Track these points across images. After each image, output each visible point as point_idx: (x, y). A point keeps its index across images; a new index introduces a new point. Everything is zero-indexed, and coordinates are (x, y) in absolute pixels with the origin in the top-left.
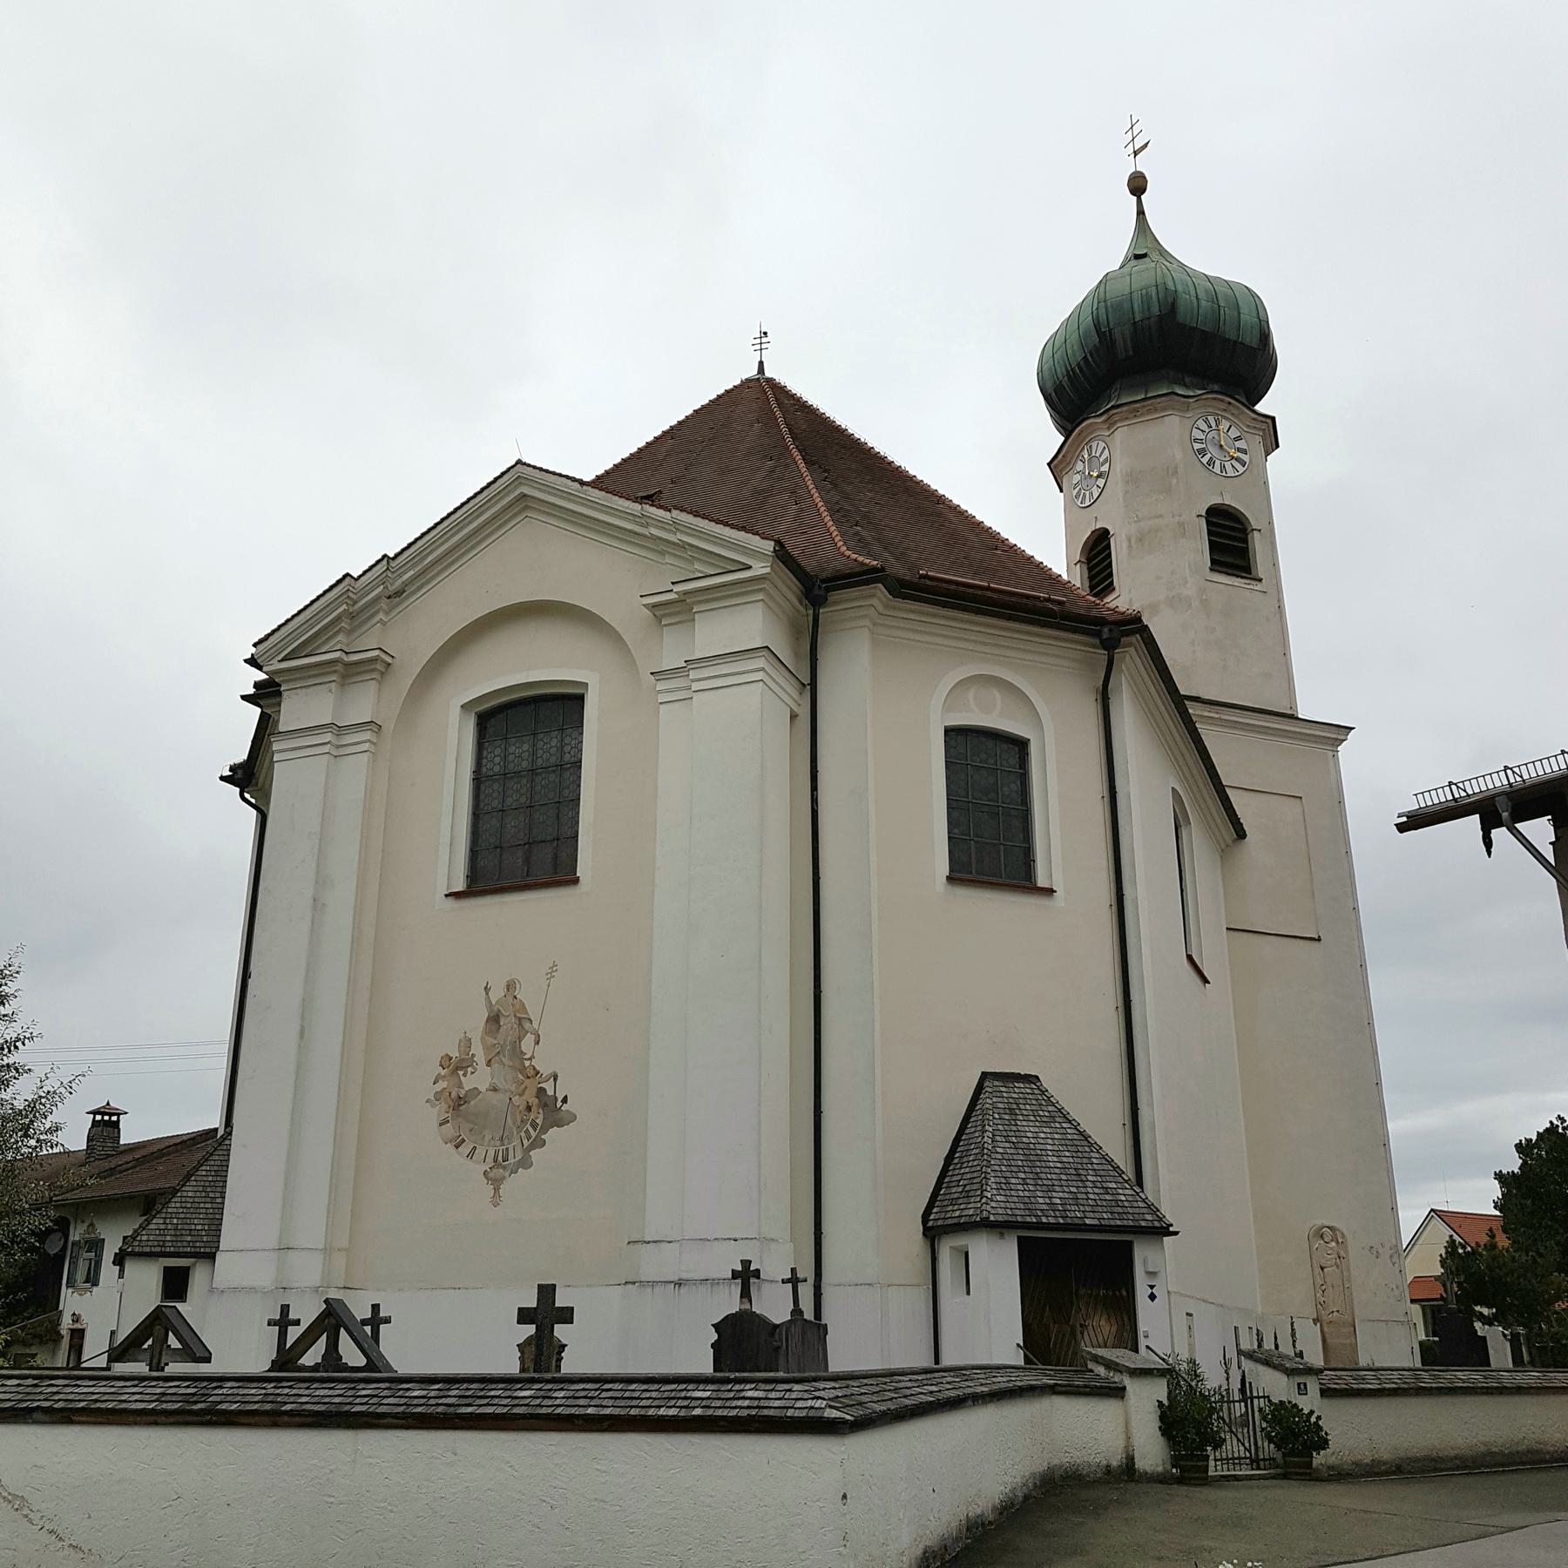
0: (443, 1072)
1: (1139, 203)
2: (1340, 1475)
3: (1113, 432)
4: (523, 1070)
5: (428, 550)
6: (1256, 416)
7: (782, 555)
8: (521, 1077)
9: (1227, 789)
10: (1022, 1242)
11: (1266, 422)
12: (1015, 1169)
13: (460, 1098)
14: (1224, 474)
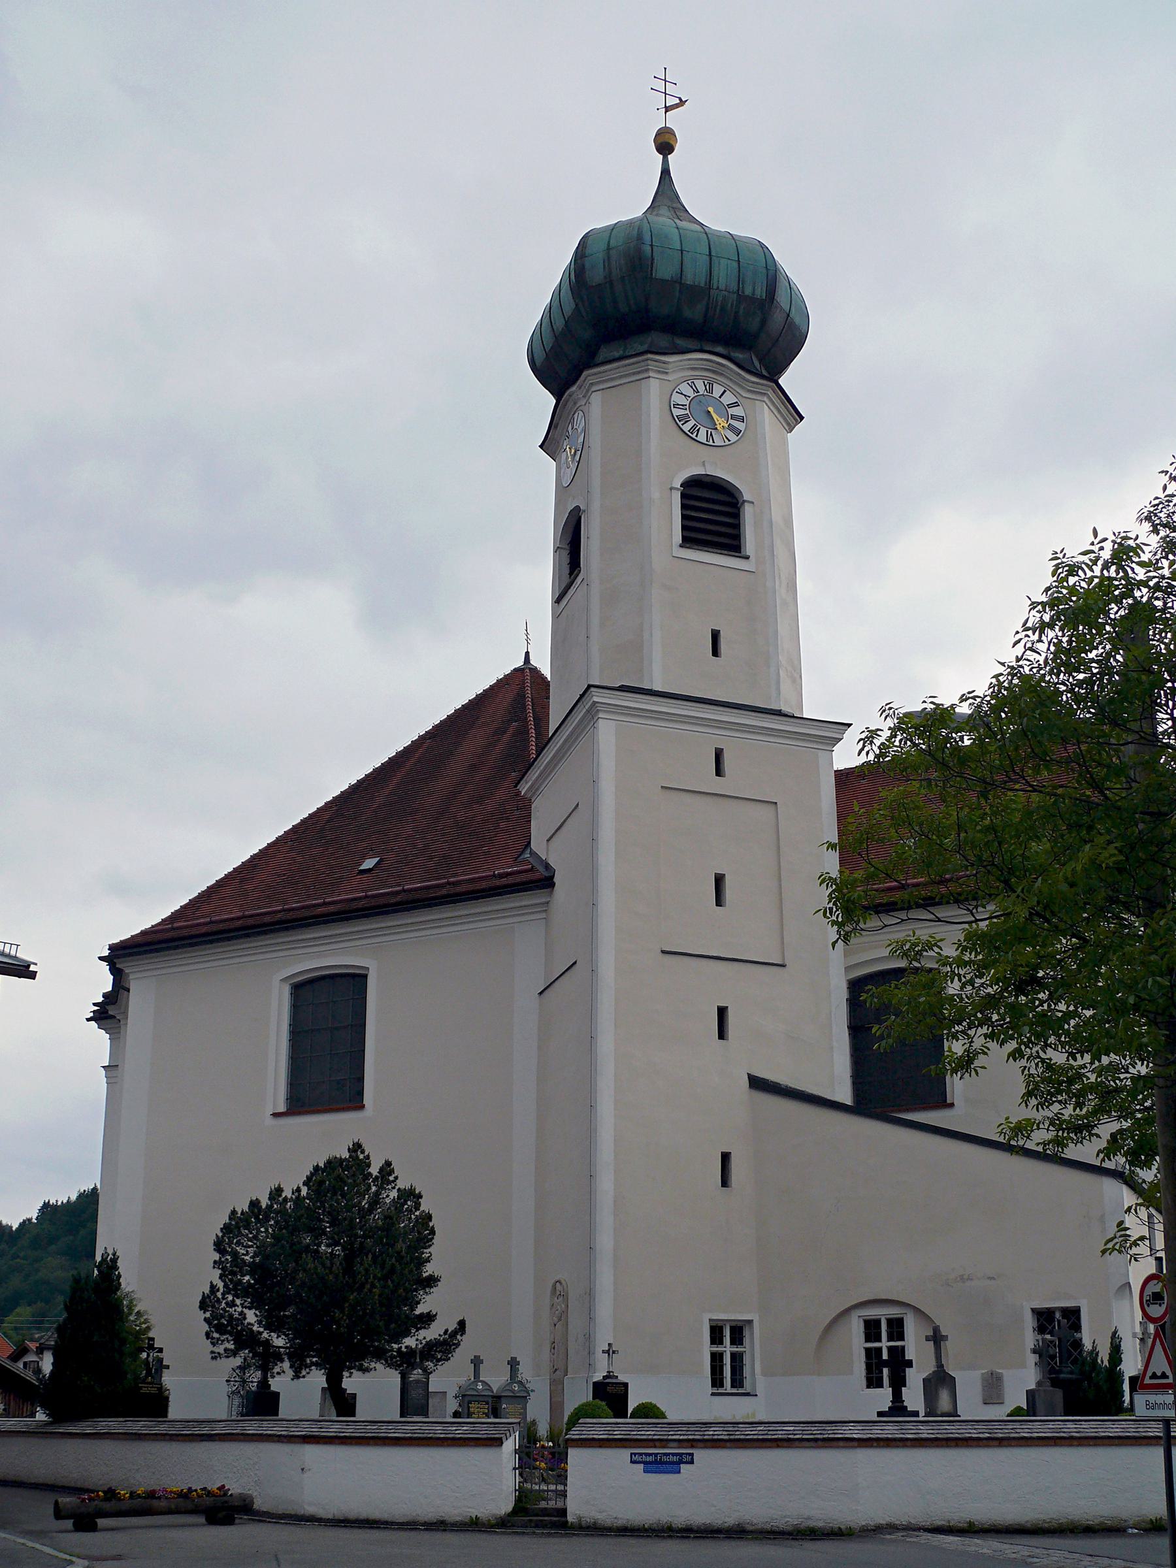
1: (665, 162)
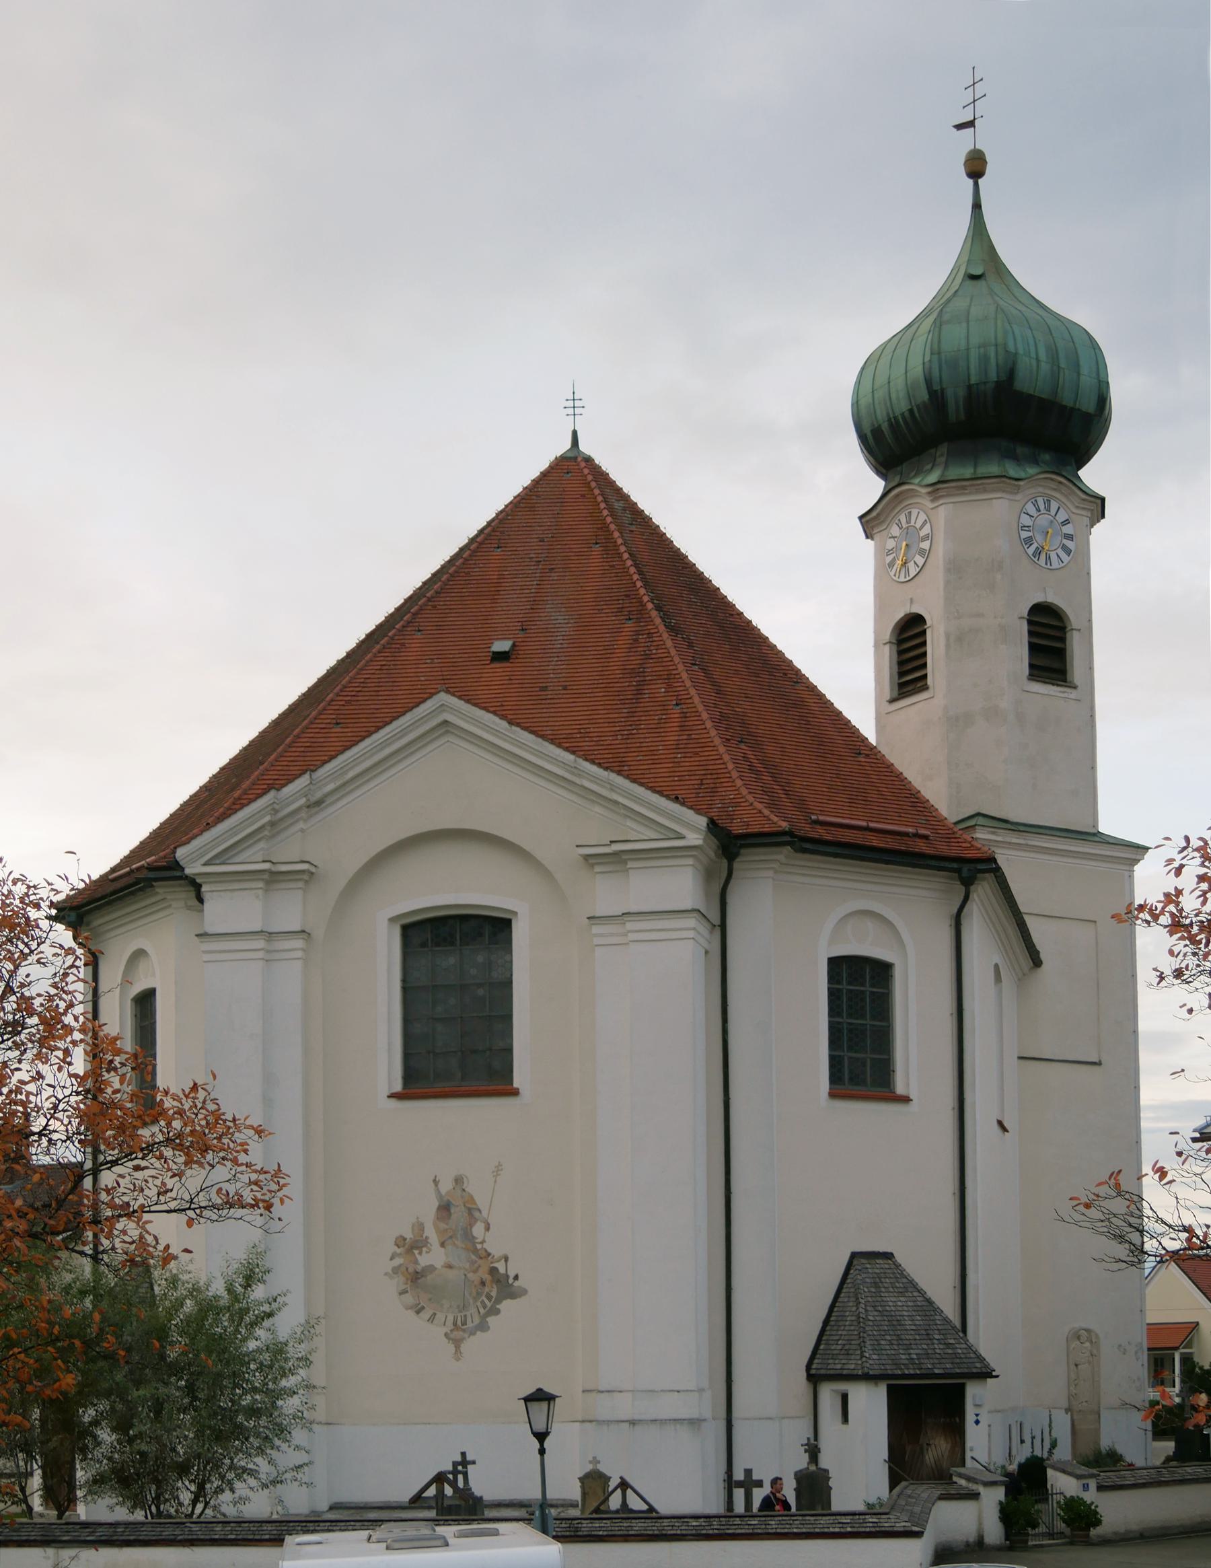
0: (399, 1251)
1: (976, 185)
2: (1106, 1542)
3: (937, 506)
4: (475, 1251)
5: (350, 766)
6: (1084, 496)
7: (714, 827)
8: (473, 1257)
9: (1024, 915)
10: (890, 1389)
11: (1095, 503)
12: (883, 1333)
13: (417, 1273)
14: (1049, 566)
